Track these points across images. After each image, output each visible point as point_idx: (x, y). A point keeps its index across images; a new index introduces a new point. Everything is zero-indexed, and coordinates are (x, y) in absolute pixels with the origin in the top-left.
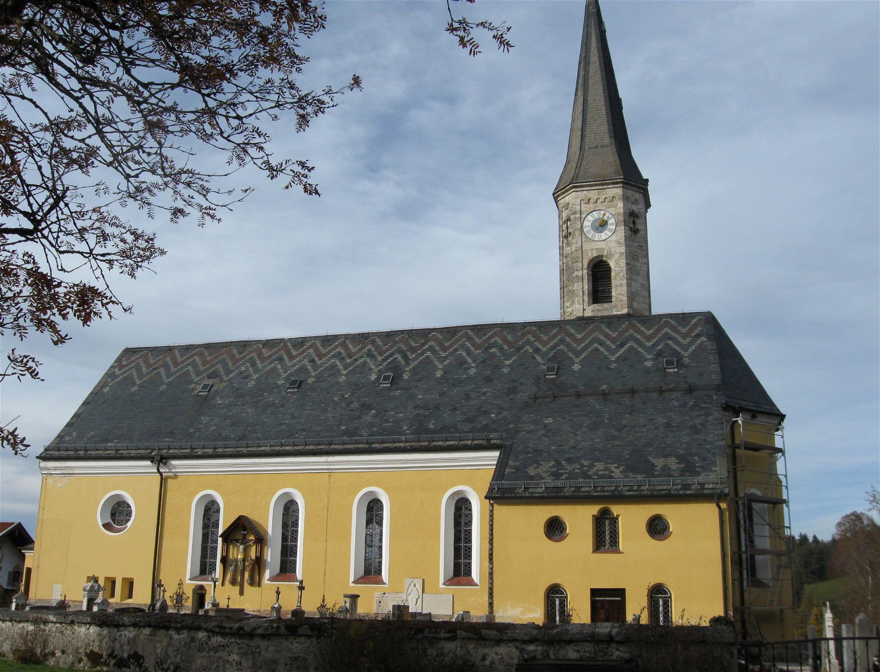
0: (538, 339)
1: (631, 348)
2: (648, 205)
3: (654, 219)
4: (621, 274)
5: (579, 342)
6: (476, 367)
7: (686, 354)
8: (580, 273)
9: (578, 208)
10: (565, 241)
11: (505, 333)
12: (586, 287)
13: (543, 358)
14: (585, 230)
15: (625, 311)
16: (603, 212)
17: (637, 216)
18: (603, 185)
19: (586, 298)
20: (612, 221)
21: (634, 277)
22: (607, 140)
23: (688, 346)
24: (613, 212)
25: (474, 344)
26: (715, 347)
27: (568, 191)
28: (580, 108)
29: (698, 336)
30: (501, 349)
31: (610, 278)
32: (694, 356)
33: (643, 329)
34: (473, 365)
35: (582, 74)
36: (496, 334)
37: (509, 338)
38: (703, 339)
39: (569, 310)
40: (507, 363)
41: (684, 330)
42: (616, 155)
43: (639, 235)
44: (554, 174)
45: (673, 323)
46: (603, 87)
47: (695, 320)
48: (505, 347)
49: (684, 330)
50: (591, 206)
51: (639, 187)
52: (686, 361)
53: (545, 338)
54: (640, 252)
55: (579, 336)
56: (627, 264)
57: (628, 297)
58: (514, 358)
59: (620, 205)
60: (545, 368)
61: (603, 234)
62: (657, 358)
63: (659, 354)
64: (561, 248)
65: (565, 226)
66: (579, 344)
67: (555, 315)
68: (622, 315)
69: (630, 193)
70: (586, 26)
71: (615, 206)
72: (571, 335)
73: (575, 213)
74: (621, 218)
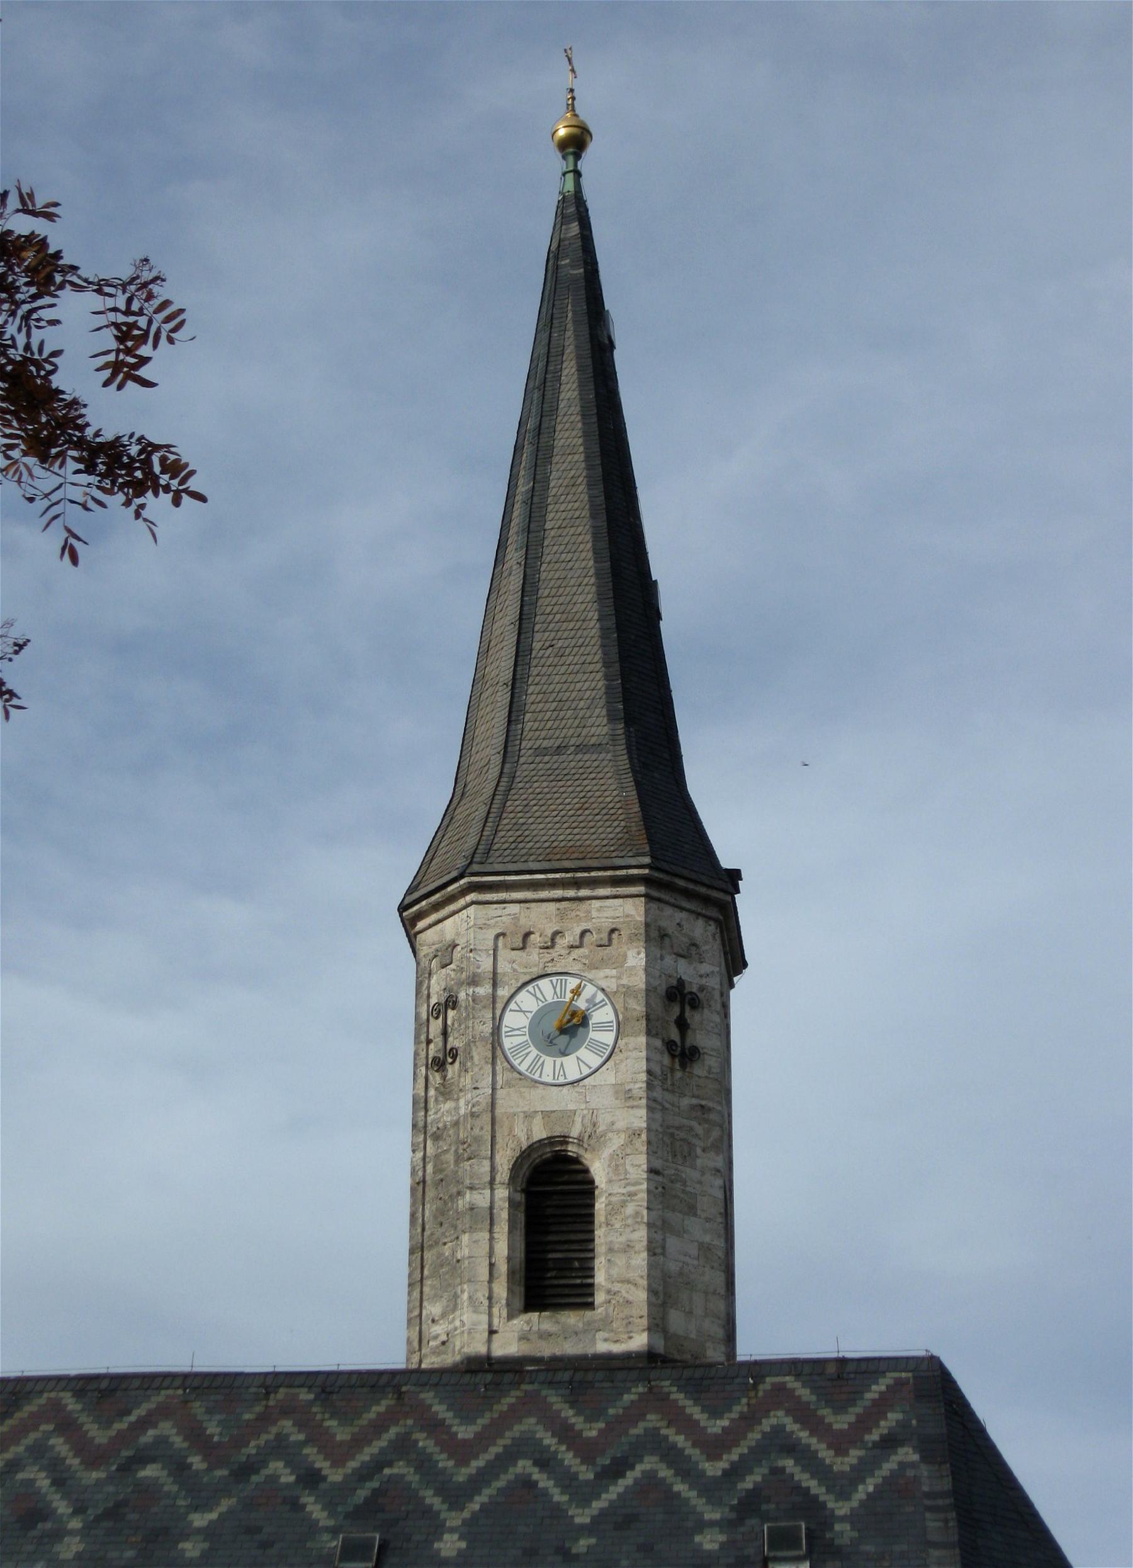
0: (319, 1437)
1: (650, 1482)
2: (735, 962)
3: (758, 1018)
4: (630, 1209)
5: (462, 1452)
6: (85, 1532)
7: (842, 1509)
8: (481, 1199)
9: (486, 964)
10: (436, 1078)
11: (198, 1408)
12: (502, 1248)
13: (330, 1506)
14: (508, 1043)
15: (639, 1341)
16: (573, 983)
17: (695, 1003)
18: (577, 884)
19: (501, 1290)
20: (603, 1015)
21: (674, 1218)
22: (599, 725)
23: (854, 1477)
24: (611, 985)
25: (82, 1446)
26: (946, 1484)
27: (452, 899)
28: (511, 611)
29: (889, 1443)
30: (180, 1468)
31: (589, 1219)
32: (871, 1516)
33: (695, 1412)
34: (75, 1524)
35: (523, 487)
36: (163, 1412)
37: (213, 1429)
38: (907, 1454)
39: (439, 1329)
40: (199, 1520)
41: (841, 1422)
42: (629, 780)
43: (698, 1070)
44: (424, 795)
45: (804, 1393)
46: (596, 537)
47: (879, 1387)
48: (196, 1462)
49: (841, 1422)
50: (534, 958)
51: (707, 900)
52: (843, 1532)
53: (342, 1434)
54: (699, 1129)
55: (465, 1432)
56: (652, 1171)
57: (652, 1291)
58: (225, 1504)
59: (636, 958)
60: (336, 1544)
61: (569, 1062)
62: (740, 1521)
63: (750, 1506)
64: (421, 1104)
65: (436, 1026)
66: (463, 1462)
67: (381, 1347)
68: (627, 1356)
69: (671, 918)
70: (548, 321)
71: (619, 962)
72: (435, 1426)
73: (474, 981)
74: (638, 1007)
